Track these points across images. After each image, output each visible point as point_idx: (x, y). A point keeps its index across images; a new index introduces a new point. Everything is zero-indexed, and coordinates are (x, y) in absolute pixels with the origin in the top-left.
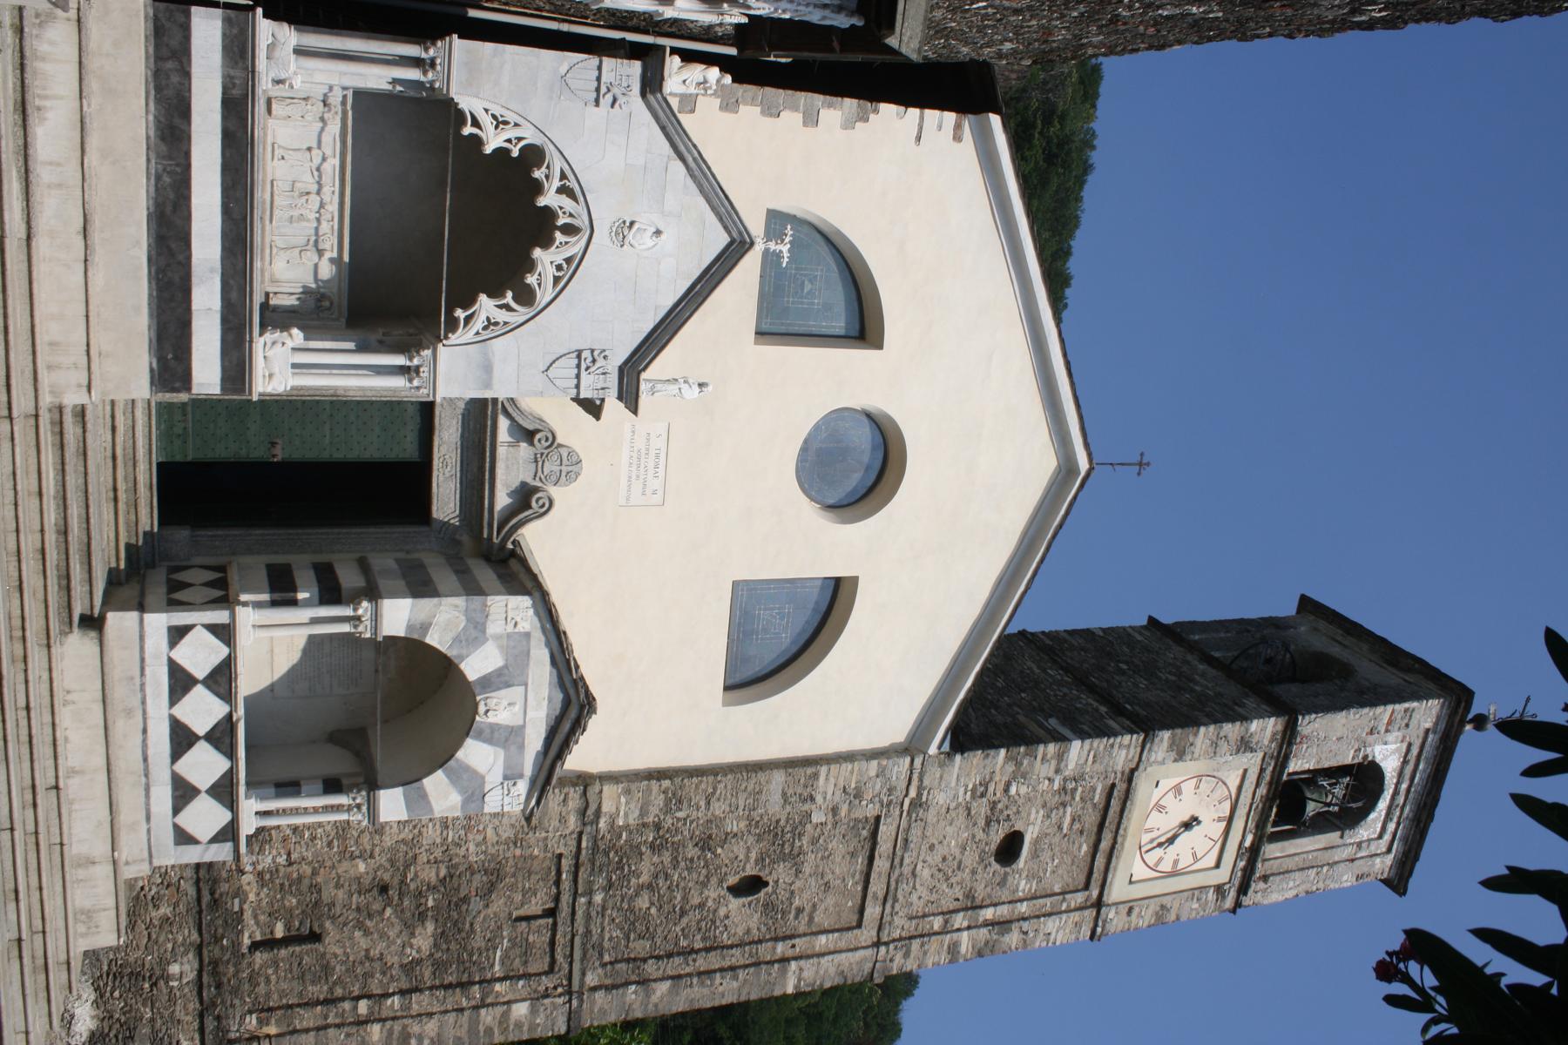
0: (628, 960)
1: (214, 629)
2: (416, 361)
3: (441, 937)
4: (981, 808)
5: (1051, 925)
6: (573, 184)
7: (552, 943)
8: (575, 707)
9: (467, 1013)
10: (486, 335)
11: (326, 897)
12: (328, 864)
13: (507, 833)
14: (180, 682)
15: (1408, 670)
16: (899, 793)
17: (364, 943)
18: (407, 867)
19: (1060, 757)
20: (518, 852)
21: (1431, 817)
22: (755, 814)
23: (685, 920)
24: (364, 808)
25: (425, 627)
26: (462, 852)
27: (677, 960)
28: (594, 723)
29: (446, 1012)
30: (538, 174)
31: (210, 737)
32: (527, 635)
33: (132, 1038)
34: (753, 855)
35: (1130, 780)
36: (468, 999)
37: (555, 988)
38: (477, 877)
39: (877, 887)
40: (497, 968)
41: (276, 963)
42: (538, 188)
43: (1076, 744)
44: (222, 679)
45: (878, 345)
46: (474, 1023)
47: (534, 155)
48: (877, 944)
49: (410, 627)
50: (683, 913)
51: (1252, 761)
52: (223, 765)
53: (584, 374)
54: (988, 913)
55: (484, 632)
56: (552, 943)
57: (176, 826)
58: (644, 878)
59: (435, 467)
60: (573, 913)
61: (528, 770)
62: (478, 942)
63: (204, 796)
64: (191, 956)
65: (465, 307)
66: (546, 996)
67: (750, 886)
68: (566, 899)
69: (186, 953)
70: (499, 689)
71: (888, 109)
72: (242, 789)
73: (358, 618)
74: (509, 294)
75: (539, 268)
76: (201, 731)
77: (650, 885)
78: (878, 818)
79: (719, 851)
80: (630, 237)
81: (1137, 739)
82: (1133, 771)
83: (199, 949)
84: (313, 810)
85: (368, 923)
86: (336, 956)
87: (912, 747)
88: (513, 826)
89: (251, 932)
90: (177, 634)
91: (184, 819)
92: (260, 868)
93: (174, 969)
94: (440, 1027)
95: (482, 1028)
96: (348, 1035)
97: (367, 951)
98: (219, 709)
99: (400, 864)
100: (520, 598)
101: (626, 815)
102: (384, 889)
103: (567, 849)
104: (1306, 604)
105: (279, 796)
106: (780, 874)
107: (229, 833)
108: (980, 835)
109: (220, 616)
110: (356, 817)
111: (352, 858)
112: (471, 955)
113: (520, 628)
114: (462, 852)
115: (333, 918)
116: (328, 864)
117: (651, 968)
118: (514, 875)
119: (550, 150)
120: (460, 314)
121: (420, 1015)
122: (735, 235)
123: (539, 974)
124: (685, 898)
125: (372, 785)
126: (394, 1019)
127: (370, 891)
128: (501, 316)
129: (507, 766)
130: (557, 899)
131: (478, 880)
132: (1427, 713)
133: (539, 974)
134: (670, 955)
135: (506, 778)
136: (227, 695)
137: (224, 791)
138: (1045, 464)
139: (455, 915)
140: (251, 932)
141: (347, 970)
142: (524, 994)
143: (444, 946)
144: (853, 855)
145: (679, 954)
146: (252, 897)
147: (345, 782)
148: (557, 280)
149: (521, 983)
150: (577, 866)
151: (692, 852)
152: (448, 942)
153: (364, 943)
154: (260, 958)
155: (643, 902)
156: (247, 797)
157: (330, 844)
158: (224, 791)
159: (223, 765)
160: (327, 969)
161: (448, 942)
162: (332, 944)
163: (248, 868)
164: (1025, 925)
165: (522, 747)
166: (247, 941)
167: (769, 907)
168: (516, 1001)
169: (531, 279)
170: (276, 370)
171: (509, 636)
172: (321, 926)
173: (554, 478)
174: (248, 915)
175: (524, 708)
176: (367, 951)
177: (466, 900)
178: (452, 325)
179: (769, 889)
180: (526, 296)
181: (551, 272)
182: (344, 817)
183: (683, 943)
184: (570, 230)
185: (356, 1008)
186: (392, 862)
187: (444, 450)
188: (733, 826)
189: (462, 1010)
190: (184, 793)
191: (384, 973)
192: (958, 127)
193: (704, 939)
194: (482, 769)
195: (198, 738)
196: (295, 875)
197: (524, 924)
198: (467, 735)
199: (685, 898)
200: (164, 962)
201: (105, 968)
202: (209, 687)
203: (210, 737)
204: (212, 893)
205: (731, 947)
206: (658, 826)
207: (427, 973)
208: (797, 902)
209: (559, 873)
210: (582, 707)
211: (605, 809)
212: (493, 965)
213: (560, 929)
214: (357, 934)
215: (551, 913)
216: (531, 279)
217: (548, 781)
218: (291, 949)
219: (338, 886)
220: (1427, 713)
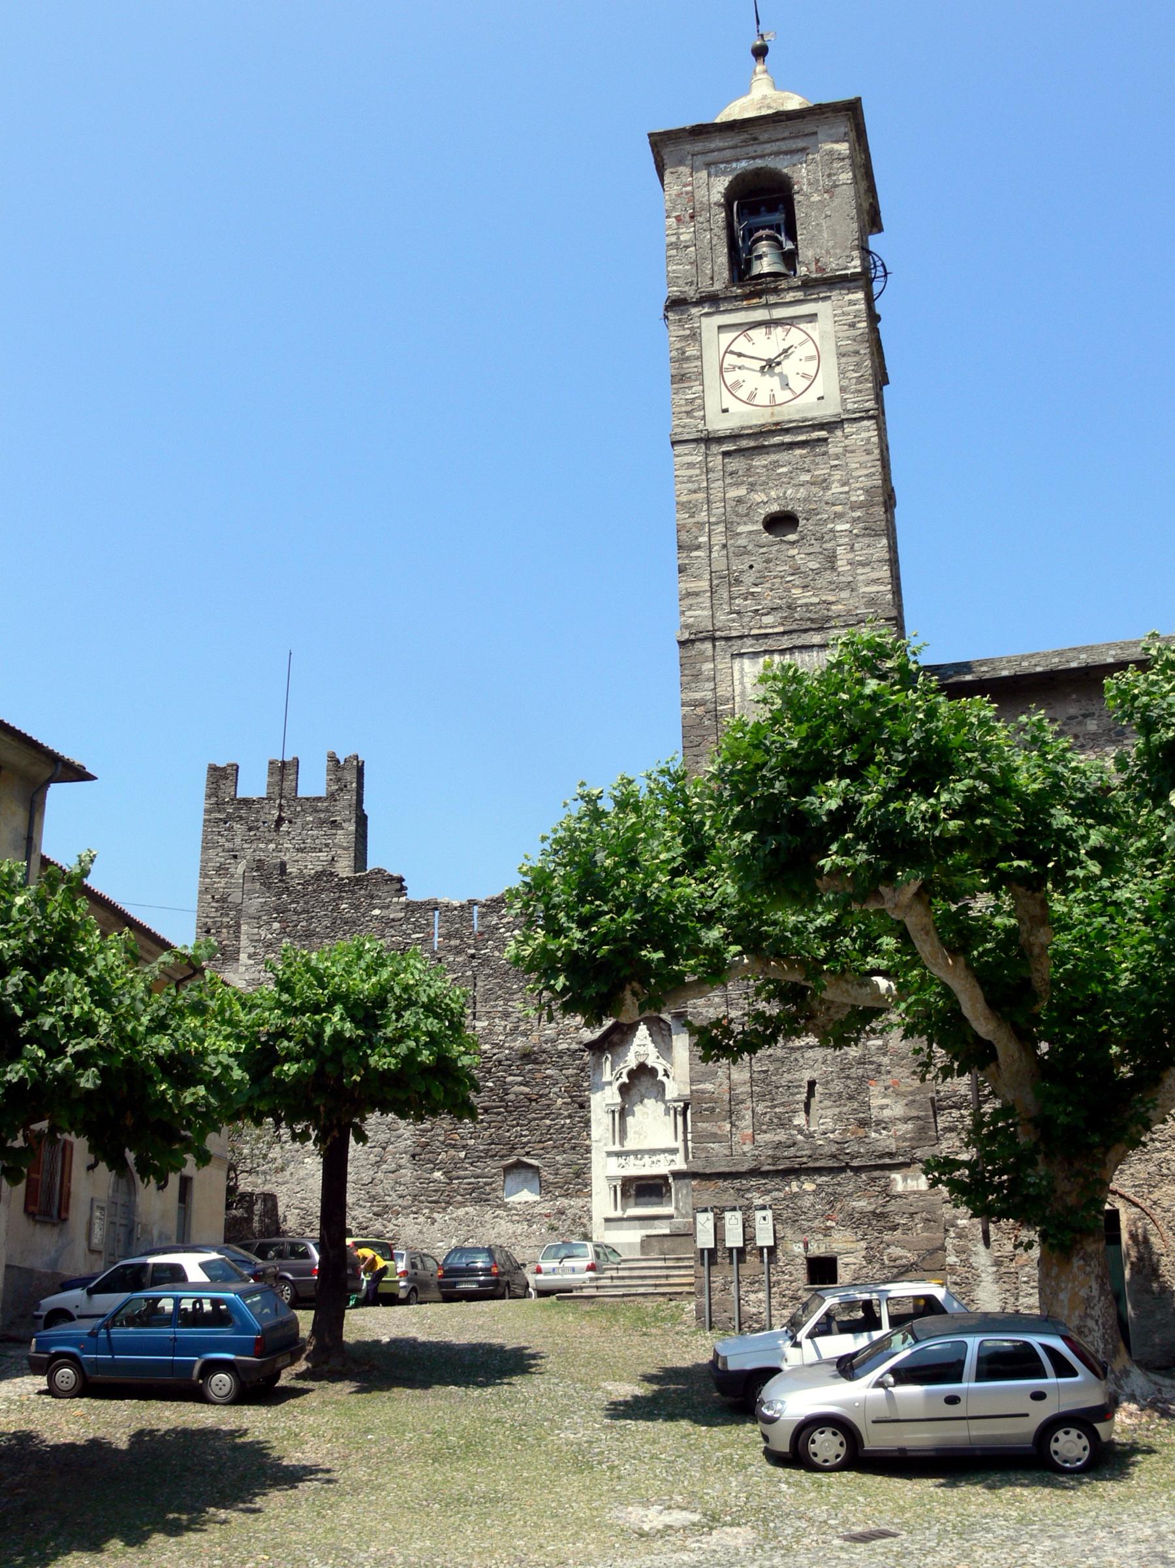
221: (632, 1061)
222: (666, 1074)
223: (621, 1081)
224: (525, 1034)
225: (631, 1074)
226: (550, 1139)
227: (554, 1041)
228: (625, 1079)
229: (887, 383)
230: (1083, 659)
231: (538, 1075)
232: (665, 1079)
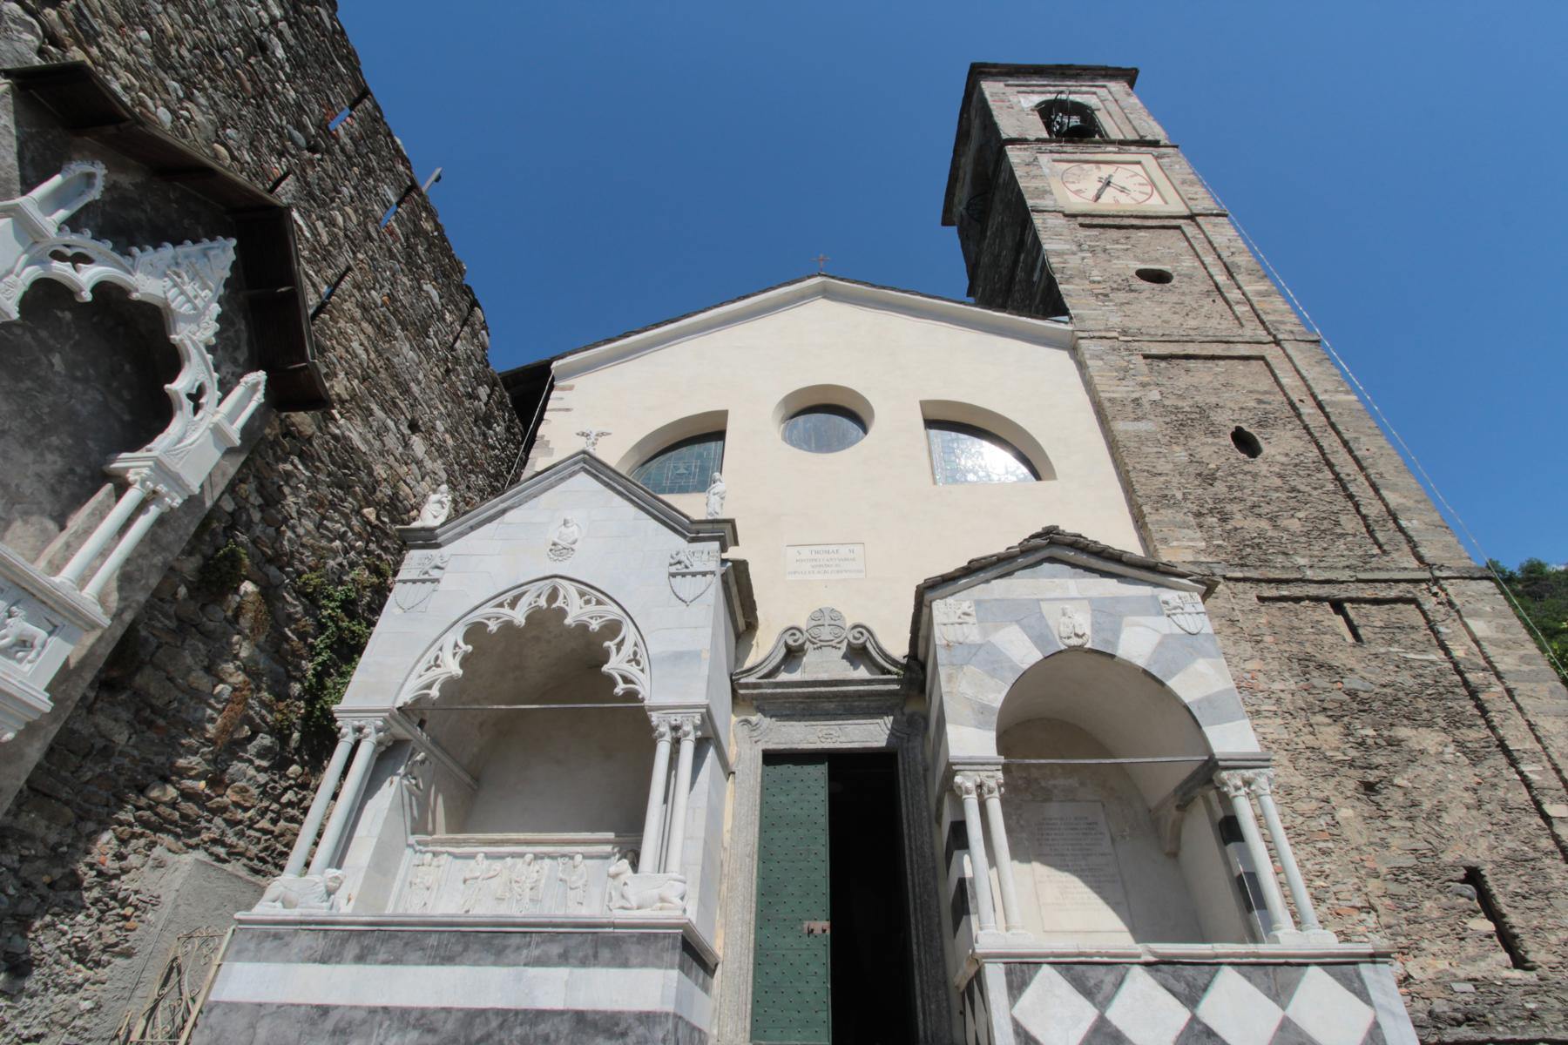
0: (1371, 532)
1: (1016, 987)
2: (664, 729)
4: (1121, 296)
5: (1218, 240)
6: (509, 597)
7: (1377, 602)
8: (1054, 547)
9: (1512, 685)
10: (644, 662)
11: (1409, 861)
12: (1355, 856)
13: (1247, 648)
15: (969, 119)
16: (1117, 344)
18: (1329, 760)
19: (1059, 254)
20: (1268, 639)
21: (1069, 67)
22: (1164, 441)
23: (1302, 488)
24: (1248, 774)
25: (983, 709)
26: (1287, 697)
27: (1352, 489)
28: (1069, 526)
29: (1519, 708)
30: (493, 626)
31: (1191, 999)
32: (978, 603)
34: (1210, 440)
35: (1074, 216)
36: (1489, 685)
37: (1435, 595)
38: (1315, 682)
40: (1432, 657)
41: (1537, 930)
42: (508, 626)
43: (1046, 247)
45: (723, 415)
47: (475, 632)
48: (1277, 342)
49: (981, 725)
50: (1293, 490)
51: (1044, 159)
52: (1229, 979)
53: (692, 570)
55: (981, 646)
56: (1377, 602)
59: (826, 746)
61: (1145, 591)
63: (1290, 1012)
65: (614, 683)
66: (1451, 604)
67: (1245, 442)
68: (1313, 590)
70: (1047, 626)
71: (542, 430)
72: (1264, 948)
73: (980, 786)
74: (607, 644)
75: (585, 618)
76: (1181, 1015)
77: (1270, 519)
78: (1146, 357)
79: (1212, 466)
80: (564, 544)
81: (1035, 216)
82: (1066, 215)
84: (1273, 852)
86: (1491, 848)
87: (1073, 350)
88: (1235, 643)
94: (1546, 714)
95: (1525, 668)
99: (1328, 767)
100: (935, 613)
101: (1192, 540)
102: (1369, 788)
103: (1251, 593)
104: (946, 221)
105: (1262, 904)
106: (1226, 420)
107: (1342, 966)
108: (1146, 294)
109: (995, 977)
110: (1262, 782)
112: (1427, 686)
113: (971, 610)
114: (1287, 697)
115: (1436, 852)
116: (1355, 856)
118: (1300, 643)
119: (475, 617)
120: (620, 688)
121: (1538, 739)
122: (577, 467)
123: (1424, 613)
124: (1276, 490)
125: (1209, 770)
127: (1378, 804)
128: (627, 649)
129: (1146, 612)
130: (1318, 599)
132: (989, 88)
133: (1424, 613)
134: (1350, 497)
135: (1160, 613)
137: (1277, 974)
138: (822, 304)
141: (1508, 832)
142: (1457, 625)
143: (1426, 715)
144: (1187, 371)
145: (1345, 489)
146: (1442, 964)
147: (1220, 814)
148: (599, 603)
149: (1442, 629)
150: (1269, 581)
154: (1536, 954)
155: (1294, 525)
156: (1276, 940)
157: (1324, 852)
159: (1229, 979)
160: (1518, 861)
162: (1480, 853)
164: (1224, 255)
165: (1117, 600)
166: (1517, 974)
168: (1471, 633)
169: (595, 625)
170: (655, 892)
171: (980, 621)
172: (1454, 867)
173: (837, 630)
175: (1070, 605)
177: (1353, 694)
178: (632, 695)
180: (612, 629)
181: (592, 608)
182: (1269, 801)
183: (1331, 487)
184: (553, 595)
186: (1326, 776)
187: (812, 738)
188: (1180, 455)
189: (1509, 691)
192: (563, 389)
194: (1156, 639)
195: (1194, 1019)
196: (1387, 901)
197: (1361, 631)
198: (1112, 656)
199: (1276, 490)
202: (1109, 999)
203: (1191, 999)
204: (1459, 1024)
205: (1320, 448)
206: (1199, 515)
207: (1472, 734)
208: (1253, 404)
210: (1052, 543)
211: (1191, 559)
212: (1432, 662)
213: (1354, 594)
214: (1446, 819)
215: (1337, 606)
216: (595, 625)
217: (1152, 568)
218: (1505, 910)
220: (989, 88)
222: (196, 397)
232: (188, 405)
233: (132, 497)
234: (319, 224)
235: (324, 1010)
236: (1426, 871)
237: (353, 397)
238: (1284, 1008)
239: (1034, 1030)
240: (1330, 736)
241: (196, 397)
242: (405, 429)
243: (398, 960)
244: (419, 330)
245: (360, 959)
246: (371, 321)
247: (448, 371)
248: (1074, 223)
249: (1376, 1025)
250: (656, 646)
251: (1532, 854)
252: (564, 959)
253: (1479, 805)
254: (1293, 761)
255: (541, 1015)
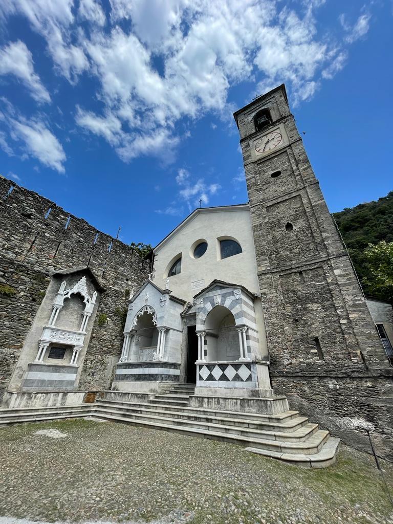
1: (200, 369)
3: (312, 302)
14: (211, 378)
17: (317, 324)
31: (223, 370)
33: (368, 405)
39: (287, 197)
40: (323, 283)
44: (210, 367)
46: (345, 285)
54: (295, 168)
57: (246, 381)
58: (288, 253)
60: (298, 267)
62: (314, 291)
64: (325, 381)
68: (293, 271)
69: (324, 383)
83: (321, 378)
85: (309, 323)
89: (317, 360)
90: (201, 378)
91: (244, 377)
92: (289, 358)
93: (331, 386)
95: (348, 282)
96: (357, 325)
97: (320, 323)
98: (217, 368)
102: (296, 321)
106: (284, 222)
111: (284, 331)
117: (318, 241)
126: (347, 310)
127: (297, 325)
130: (295, 273)
131: (291, 295)
136: (214, 366)
139: (303, 300)
140: (317, 360)
150: (282, 271)
151: (279, 244)
152: (314, 299)
153: (317, 324)
154: (326, 357)
158: (237, 366)
160: (329, 335)
161: (314, 299)
162: (319, 335)
163: (289, 362)
167: (295, 219)
172: (311, 338)
174: (309, 361)
176: (320, 323)
179: (289, 222)
180: (154, 313)
185: (344, 324)
190: (237, 378)
191: (329, 317)
193: (308, 230)
195: (223, 373)
200: (328, 391)
201: (334, 412)
203: (223, 370)
209: (286, 275)
210: (215, 283)
211: (265, 269)
215: (300, 273)
219: (295, 334)
221: (75, 290)
222: (88, 301)
223: (66, 296)
224: (16, 254)
225: (73, 295)
226: (5, 311)
227: (33, 264)
228: (69, 296)
229: (215, 280)
230: (85, 56)
231: (15, 276)
232: (87, 302)
233: (85, 317)
234: (99, 260)
235: (126, 375)
236: (304, 340)
237: (114, 282)
238: (237, 374)
239: (202, 375)
240: (289, 308)
241: (88, 301)
242: (126, 281)
243: (132, 368)
244: (122, 264)
245: (128, 368)
246: (113, 268)
247: (131, 266)
248: (256, 165)
249: (251, 374)
250: (158, 316)
251: (334, 333)
252: (148, 367)
253: (323, 322)
254: (276, 317)
255: (146, 375)
